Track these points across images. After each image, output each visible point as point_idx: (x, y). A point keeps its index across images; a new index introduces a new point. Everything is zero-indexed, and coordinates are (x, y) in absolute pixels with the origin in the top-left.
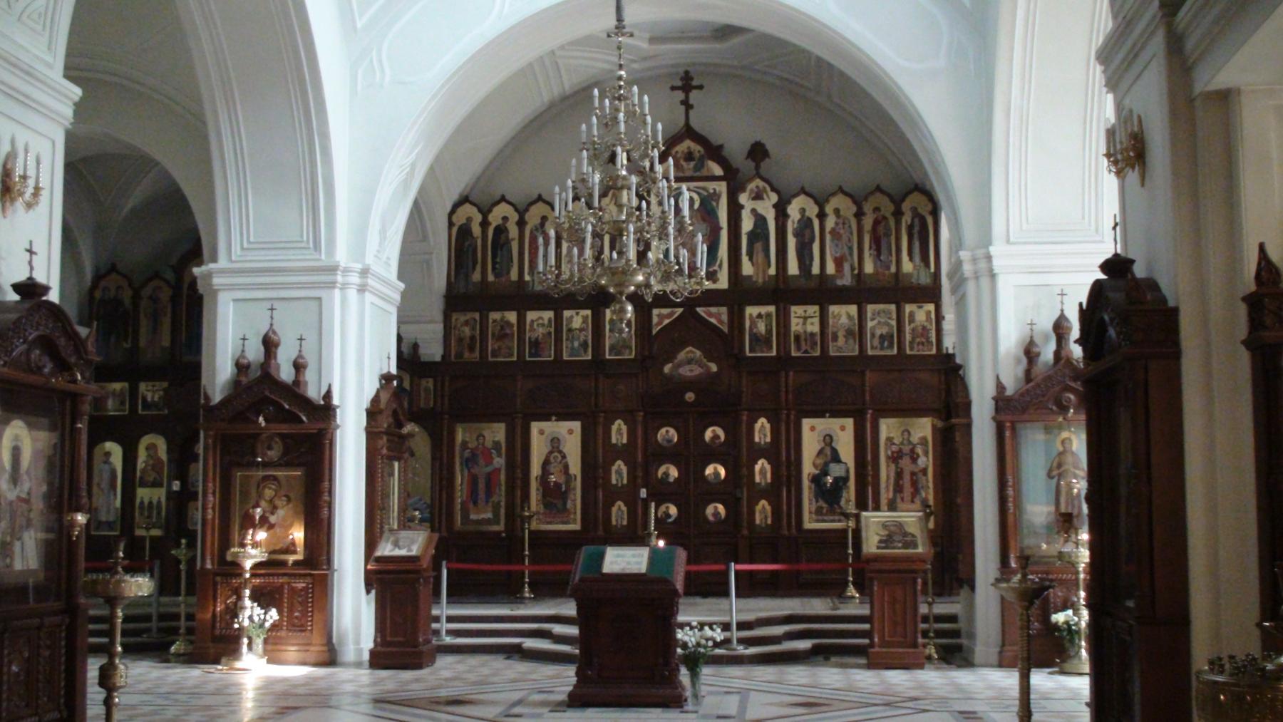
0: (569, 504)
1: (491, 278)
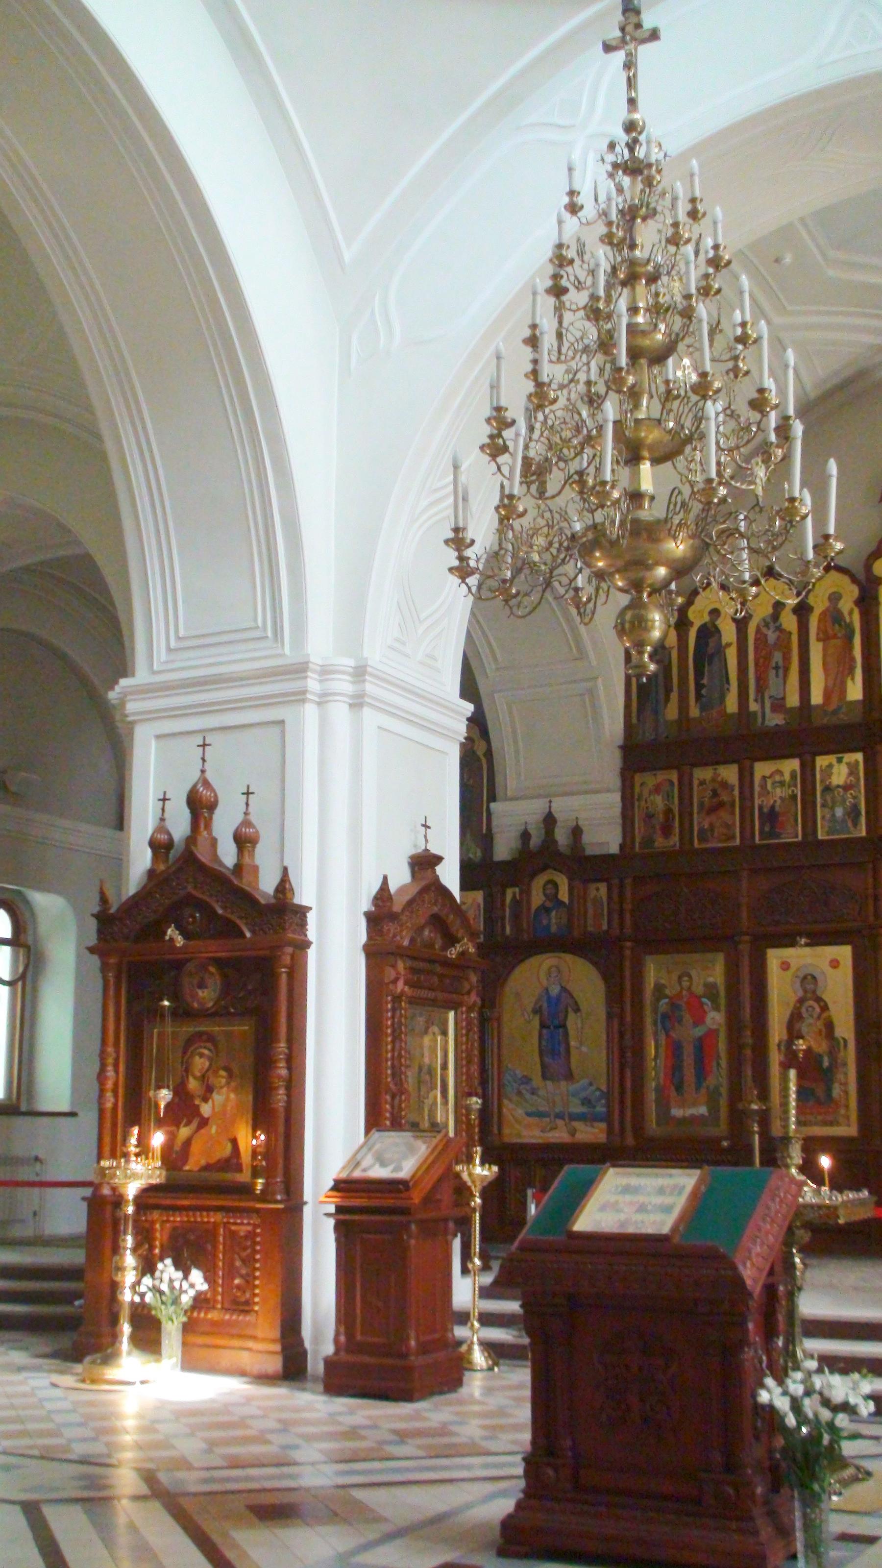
0: (836, 1091)
1: (694, 711)
